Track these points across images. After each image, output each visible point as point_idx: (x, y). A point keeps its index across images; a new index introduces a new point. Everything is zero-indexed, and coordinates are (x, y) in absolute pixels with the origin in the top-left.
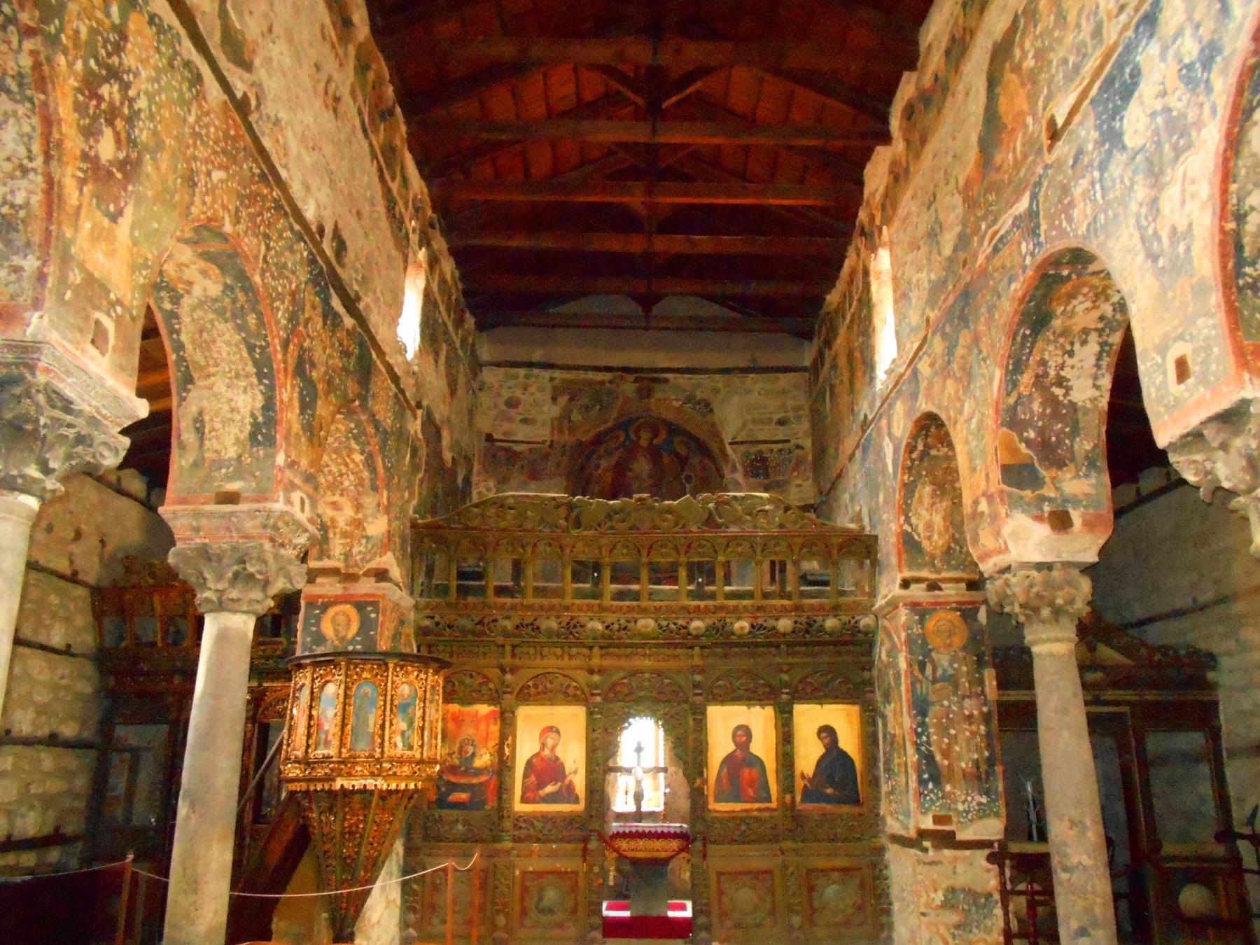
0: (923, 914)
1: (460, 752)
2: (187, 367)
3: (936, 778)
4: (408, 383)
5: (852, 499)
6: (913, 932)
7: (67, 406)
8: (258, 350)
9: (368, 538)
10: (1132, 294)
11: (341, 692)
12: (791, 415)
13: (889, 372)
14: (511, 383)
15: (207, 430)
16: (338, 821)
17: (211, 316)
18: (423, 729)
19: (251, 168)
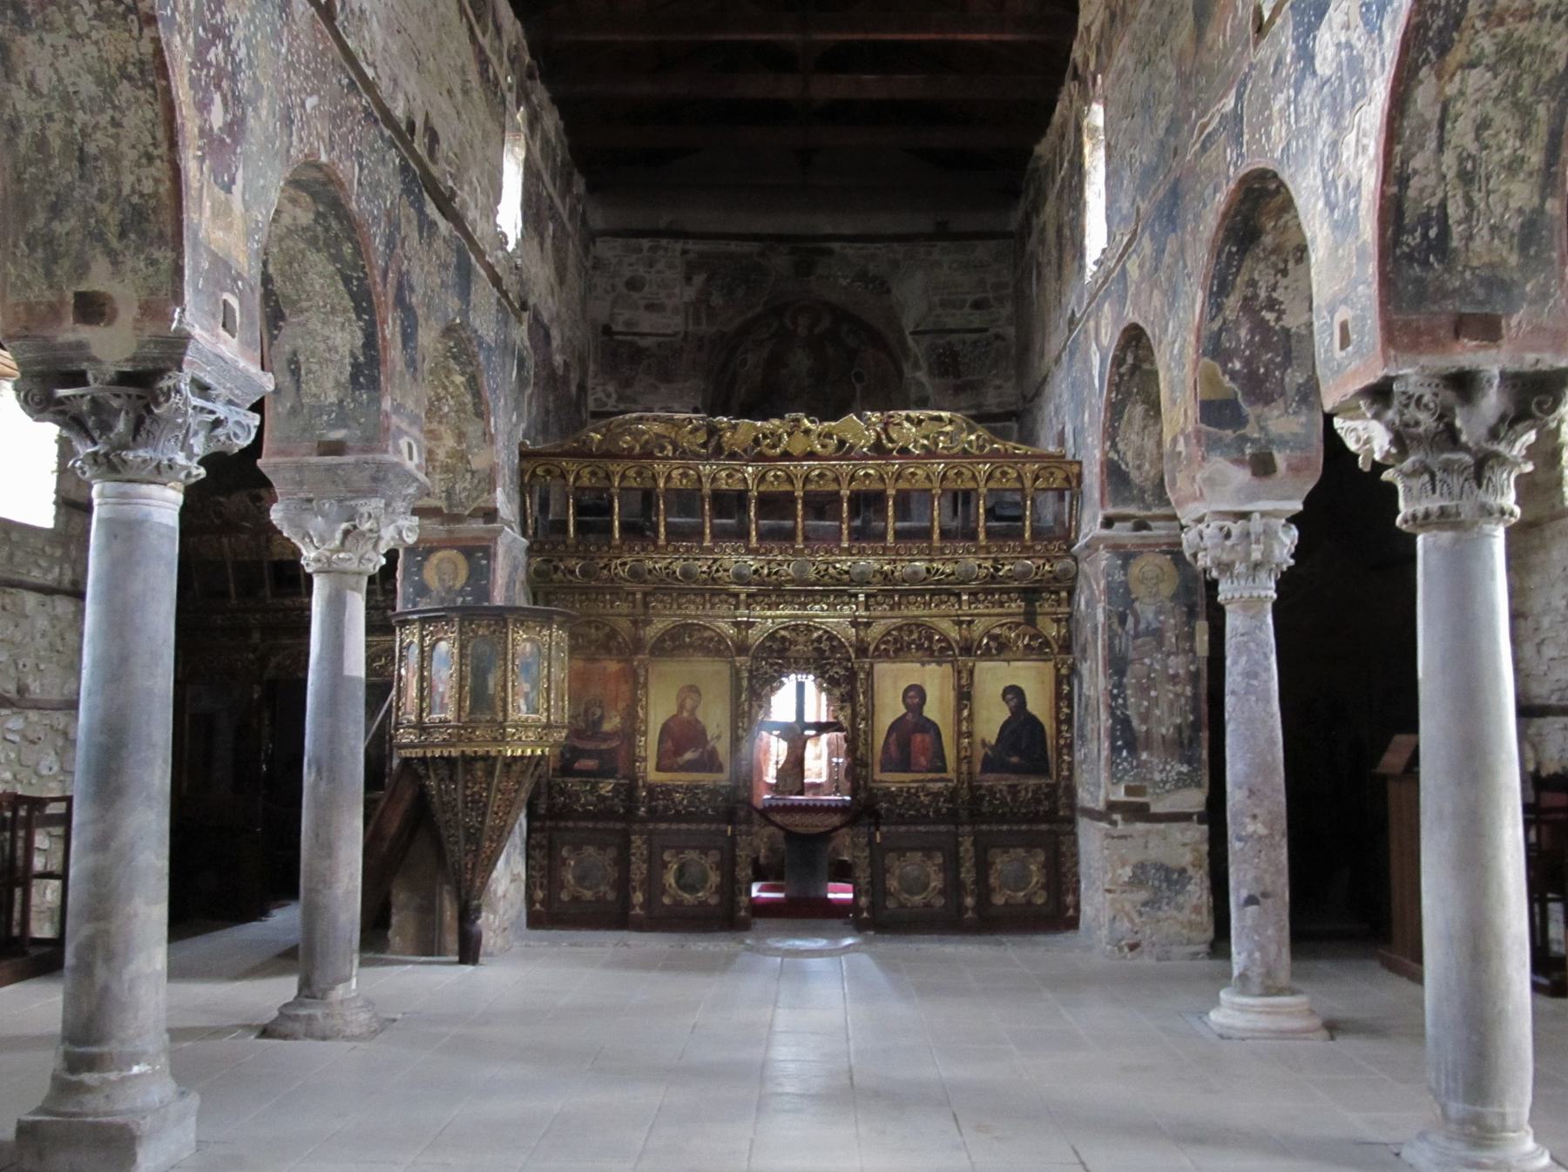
0: (1109, 891)
2: (277, 302)
4: (509, 281)
6: (1098, 910)
8: (355, 283)
9: (473, 473)
12: (990, 295)
13: (1098, 263)
14: (634, 258)
15: (303, 372)
17: (302, 245)
18: (548, 690)
19: (340, 81)
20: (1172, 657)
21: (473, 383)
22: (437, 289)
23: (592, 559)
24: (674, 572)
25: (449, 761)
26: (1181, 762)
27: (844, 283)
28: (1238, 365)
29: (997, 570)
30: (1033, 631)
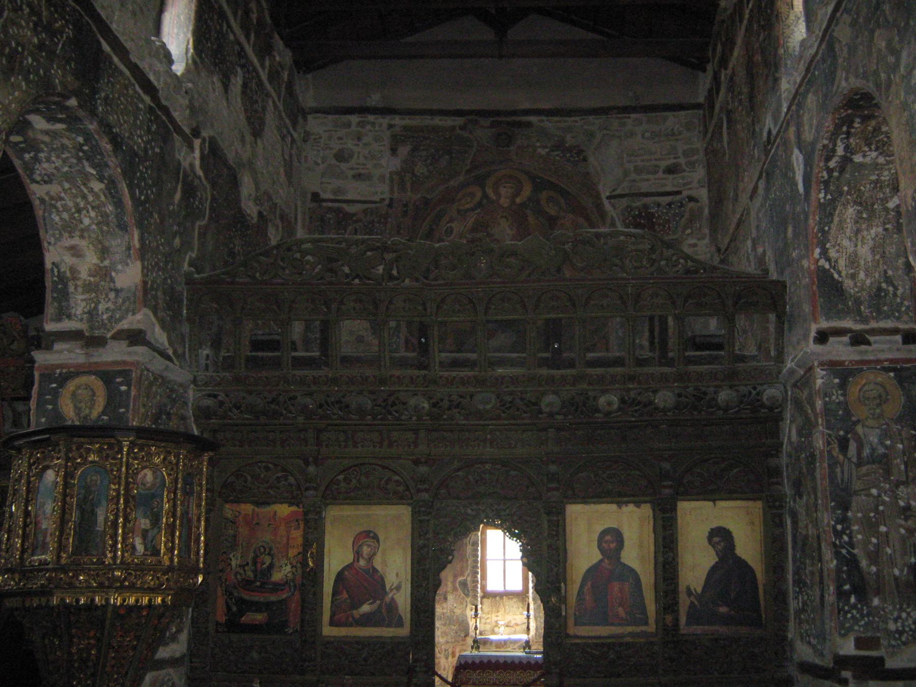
1: (255, 563)
3: (861, 590)
9: (117, 291)
12: (682, 160)
27: (543, 152)
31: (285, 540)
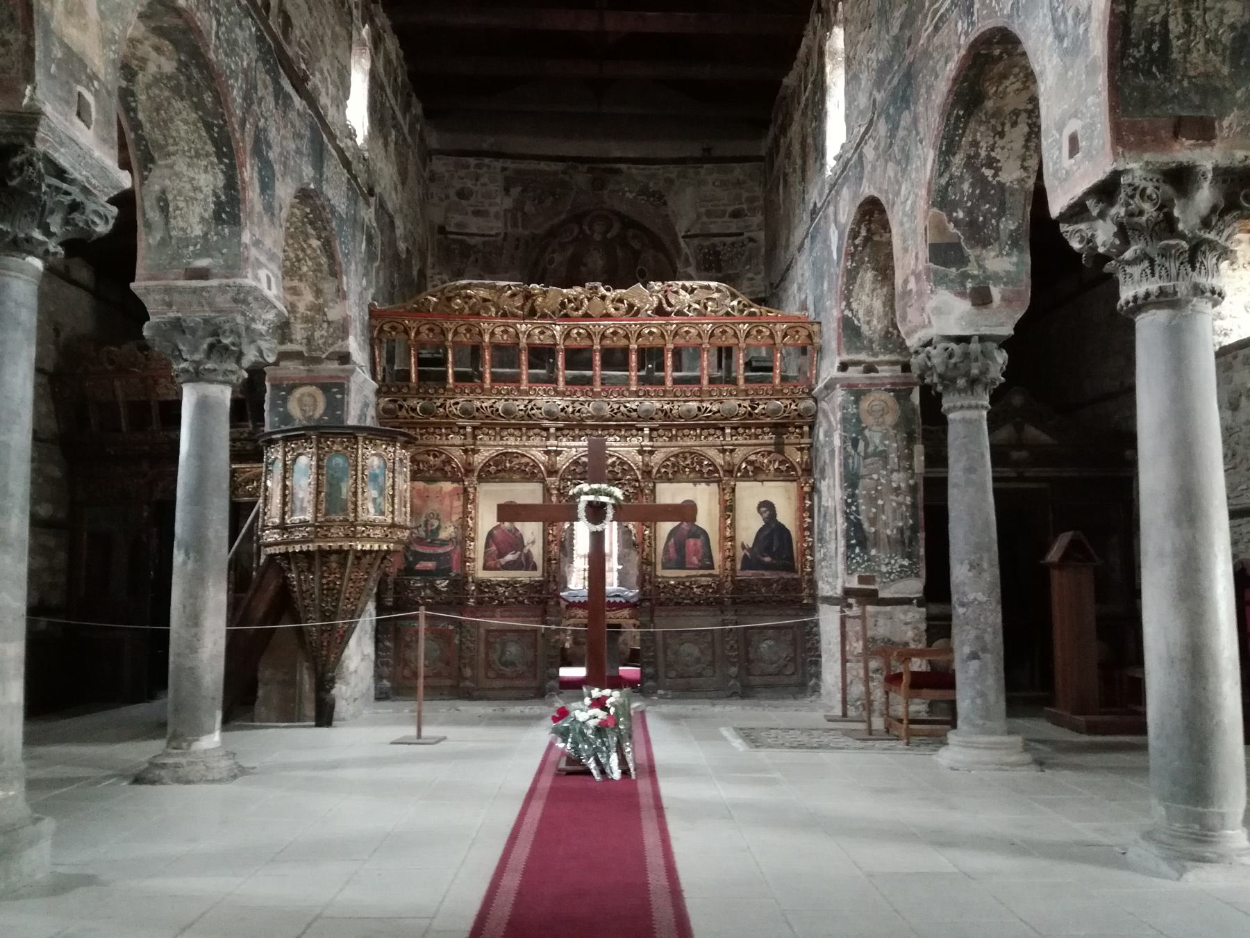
1: (426, 525)
2: (146, 146)
4: (358, 167)
5: (800, 289)
7: (60, 173)
8: (216, 129)
9: (329, 323)
10: (1041, 73)
11: (314, 463)
12: (745, 206)
13: (838, 158)
14: (462, 173)
15: (171, 209)
16: (317, 579)
17: (167, 93)
18: (393, 496)
20: (895, 474)
21: (328, 247)
22: (292, 153)
23: (431, 399)
24: (497, 410)
25: (308, 554)
26: (903, 558)
28: (961, 215)
29: (753, 408)
30: (781, 458)
31: (449, 509)
